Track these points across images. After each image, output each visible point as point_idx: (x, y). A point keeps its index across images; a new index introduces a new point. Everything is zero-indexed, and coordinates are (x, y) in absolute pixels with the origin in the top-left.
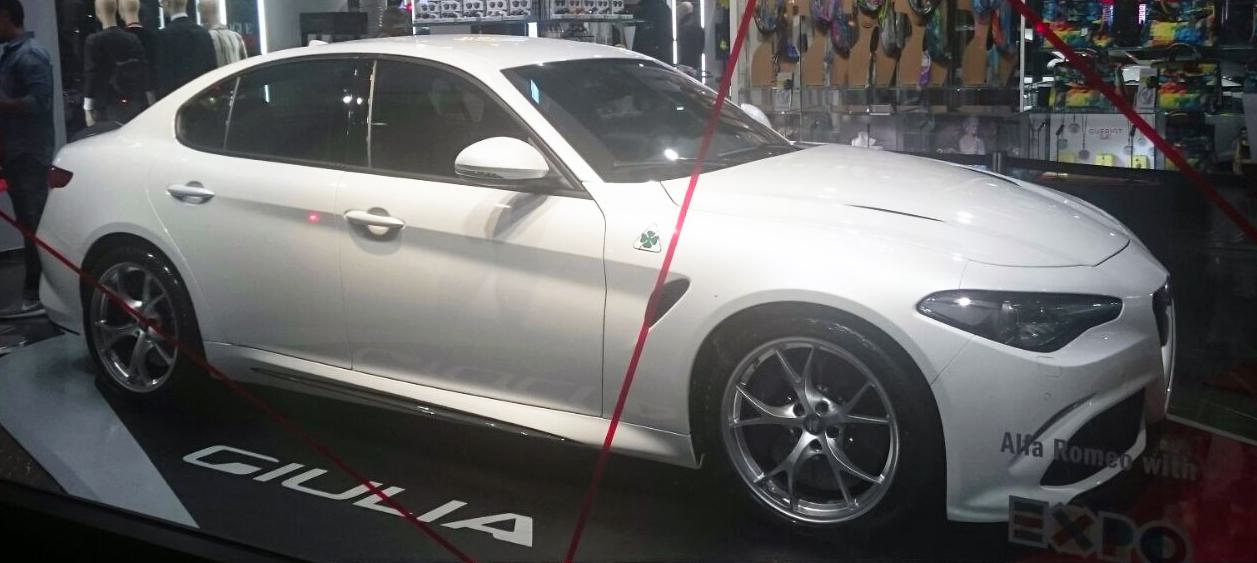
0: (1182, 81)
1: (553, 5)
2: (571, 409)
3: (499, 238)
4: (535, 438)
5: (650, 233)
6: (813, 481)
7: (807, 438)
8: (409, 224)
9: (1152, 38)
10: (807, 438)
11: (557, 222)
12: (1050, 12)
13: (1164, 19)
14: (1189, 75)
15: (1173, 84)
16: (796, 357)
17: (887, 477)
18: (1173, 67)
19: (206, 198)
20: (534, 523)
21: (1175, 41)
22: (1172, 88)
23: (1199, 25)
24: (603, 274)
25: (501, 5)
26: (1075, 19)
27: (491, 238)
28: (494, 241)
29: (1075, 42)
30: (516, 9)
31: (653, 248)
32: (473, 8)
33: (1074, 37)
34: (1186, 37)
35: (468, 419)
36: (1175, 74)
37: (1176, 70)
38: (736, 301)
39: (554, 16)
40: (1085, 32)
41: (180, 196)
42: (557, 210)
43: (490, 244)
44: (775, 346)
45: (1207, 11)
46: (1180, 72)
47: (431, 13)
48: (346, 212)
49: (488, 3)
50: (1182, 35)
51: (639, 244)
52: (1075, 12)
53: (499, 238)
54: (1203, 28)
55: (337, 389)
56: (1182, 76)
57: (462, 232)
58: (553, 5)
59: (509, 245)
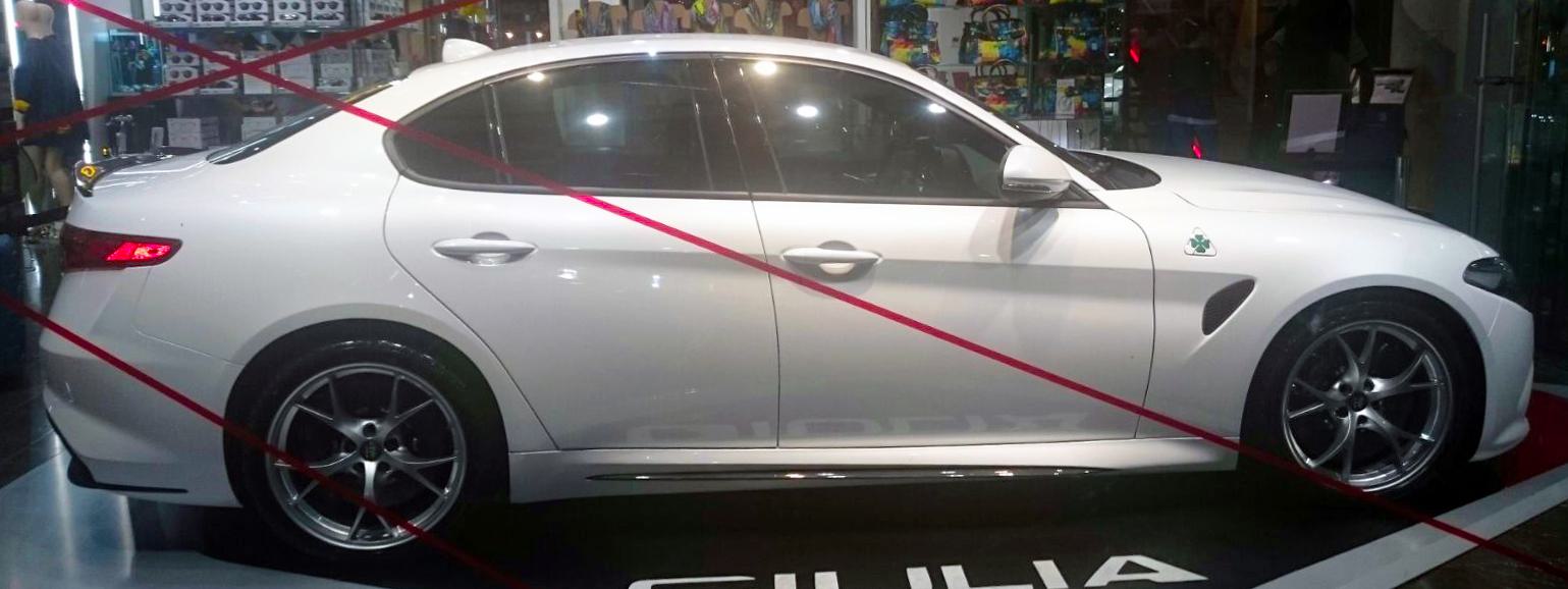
0: (1002, 93)
1: (367, 8)
2: (1070, 437)
3: (1019, 260)
4: (1038, 477)
5: (1200, 237)
6: (1371, 450)
7: (370, 467)
8: (887, 256)
9: (981, 55)
10: (370, 467)
11: (1080, 234)
12: (892, 30)
13: (986, 38)
14: (1008, 88)
15: (995, 96)
16: (319, 399)
17: (453, 490)
18: (994, 81)
19: (517, 255)
20: (780, 572)
21: (1001, 57)
22: (994, 100)
23: (1016, 43)
24: (1153, 284)
25: (296, 6)
26: (915, 37)
27: (1009, 262)
28: (1012, 265)
29: (918, 58)
30: (320, 12)
31: (1208, 251)
32: (251, 10)
33: (917, 54)
34: (1008, 54)
35: (915, 474)
36: (996, 87)
37: (997, 84)
38: (1310, 294)
39: (370, 23)
40: (925, 49)
41: (463, 255)
42: (1069, 223)
43: (1012, 271)
44: (298, 400)
45: (1019, 32)
46: (1000, 85)
47: (181, 15)
48: (783, 251)
49: (237, 3)
50: (1005, 54)
51: (1192, 250)
52: (915, 30)
53: (1019, 260)
54: (1020, 47)
55: (740, 476)
56: (1003, 89)
57: (967, 258)
58: (367, 8)
59: (1033, 266)
